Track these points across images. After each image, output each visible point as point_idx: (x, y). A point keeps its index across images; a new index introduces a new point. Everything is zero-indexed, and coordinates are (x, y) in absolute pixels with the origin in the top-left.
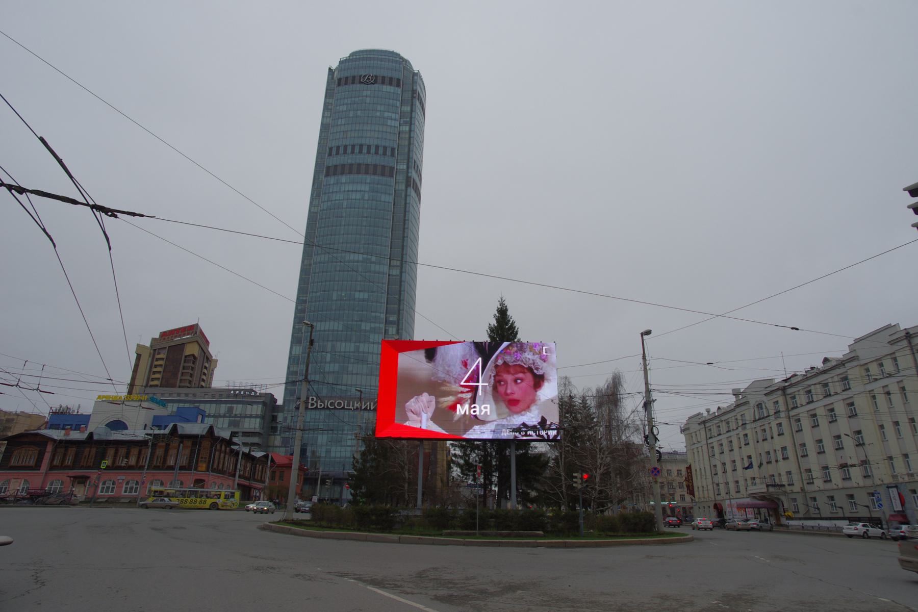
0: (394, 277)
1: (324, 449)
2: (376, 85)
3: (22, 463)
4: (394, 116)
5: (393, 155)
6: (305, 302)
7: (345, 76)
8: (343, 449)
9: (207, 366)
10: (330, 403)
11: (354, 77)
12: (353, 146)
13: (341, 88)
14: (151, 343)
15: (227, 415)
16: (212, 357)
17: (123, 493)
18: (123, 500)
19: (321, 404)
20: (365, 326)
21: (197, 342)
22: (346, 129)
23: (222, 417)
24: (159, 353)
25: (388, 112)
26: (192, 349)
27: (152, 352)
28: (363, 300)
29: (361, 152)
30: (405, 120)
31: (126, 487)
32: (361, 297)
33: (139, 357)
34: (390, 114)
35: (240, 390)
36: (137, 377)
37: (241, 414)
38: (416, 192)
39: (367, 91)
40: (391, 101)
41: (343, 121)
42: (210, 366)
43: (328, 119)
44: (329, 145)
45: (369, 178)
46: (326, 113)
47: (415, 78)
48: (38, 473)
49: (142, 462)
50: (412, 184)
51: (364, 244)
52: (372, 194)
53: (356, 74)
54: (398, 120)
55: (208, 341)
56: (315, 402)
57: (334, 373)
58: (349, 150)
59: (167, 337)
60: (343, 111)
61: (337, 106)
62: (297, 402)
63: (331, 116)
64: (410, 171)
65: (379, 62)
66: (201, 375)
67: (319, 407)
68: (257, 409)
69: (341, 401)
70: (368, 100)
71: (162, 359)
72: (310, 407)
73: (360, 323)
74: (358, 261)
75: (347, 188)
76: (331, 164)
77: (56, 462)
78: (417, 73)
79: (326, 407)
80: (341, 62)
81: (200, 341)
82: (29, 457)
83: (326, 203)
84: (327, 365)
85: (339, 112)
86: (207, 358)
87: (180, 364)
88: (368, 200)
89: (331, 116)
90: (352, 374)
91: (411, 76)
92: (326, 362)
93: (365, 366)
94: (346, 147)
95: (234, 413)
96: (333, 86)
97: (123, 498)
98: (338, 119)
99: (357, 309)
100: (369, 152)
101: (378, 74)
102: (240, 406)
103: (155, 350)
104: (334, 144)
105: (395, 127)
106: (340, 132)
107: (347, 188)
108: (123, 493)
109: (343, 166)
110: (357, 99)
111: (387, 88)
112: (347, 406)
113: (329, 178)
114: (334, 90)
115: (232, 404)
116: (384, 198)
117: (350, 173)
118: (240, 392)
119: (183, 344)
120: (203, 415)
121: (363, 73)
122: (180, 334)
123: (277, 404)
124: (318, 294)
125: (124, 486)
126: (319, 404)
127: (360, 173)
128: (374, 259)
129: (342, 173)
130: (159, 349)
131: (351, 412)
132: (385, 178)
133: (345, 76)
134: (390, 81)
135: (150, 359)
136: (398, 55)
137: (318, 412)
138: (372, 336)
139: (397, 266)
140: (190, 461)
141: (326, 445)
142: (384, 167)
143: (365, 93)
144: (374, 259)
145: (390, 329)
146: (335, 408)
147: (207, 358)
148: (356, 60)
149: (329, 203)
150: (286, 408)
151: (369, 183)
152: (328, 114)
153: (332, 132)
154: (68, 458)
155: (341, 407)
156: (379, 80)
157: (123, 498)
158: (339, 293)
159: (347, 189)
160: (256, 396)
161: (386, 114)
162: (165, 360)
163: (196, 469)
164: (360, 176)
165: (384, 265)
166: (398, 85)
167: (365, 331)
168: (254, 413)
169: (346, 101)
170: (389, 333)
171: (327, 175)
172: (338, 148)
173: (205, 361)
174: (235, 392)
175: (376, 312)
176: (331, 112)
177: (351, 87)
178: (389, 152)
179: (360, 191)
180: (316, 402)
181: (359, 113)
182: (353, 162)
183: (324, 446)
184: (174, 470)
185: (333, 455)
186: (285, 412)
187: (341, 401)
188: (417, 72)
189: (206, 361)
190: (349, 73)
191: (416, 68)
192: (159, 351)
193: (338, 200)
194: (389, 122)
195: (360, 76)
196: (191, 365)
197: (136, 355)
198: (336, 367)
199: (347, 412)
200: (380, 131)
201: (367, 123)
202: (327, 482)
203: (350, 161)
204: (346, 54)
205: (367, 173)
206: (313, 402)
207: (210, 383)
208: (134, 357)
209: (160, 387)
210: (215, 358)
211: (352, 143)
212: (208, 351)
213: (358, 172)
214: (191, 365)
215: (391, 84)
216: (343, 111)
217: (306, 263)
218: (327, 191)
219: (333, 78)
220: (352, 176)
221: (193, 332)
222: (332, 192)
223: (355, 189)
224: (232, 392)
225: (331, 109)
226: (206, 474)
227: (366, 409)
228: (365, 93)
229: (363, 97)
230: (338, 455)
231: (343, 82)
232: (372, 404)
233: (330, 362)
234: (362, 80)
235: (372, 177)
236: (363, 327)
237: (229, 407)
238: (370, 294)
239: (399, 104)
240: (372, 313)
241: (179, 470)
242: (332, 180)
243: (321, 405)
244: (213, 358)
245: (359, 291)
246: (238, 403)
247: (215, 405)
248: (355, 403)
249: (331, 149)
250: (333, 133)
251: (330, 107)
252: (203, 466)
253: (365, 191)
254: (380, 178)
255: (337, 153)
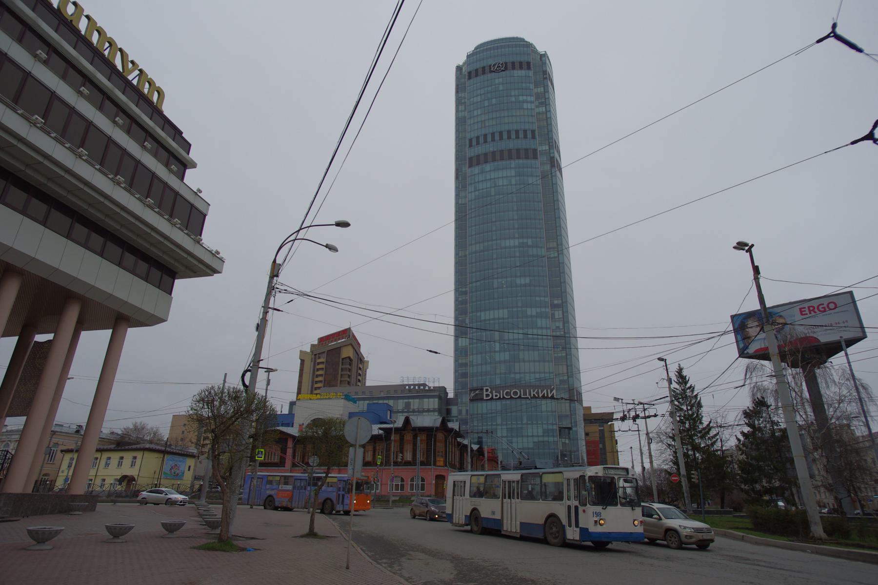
2: (507, 72)
3: (268, 460)
4: (529, 99)
5: (534, 137)
6: (465, 293)
11: (484, 68)
12: (493, 134)
13: (472, 80)
14: (311, 349)
15: (406, 410)
16: (364, 358)
19: (496, 394)
21: (351, 344)
22: (483, 119)
24: (319, 358)
25: (523, 96)
26: (347, 352)
27: (313, 356)
28: (525, 285)
29: (501, 138)
30: (540, 101)
32: (523, 282)
33: (302, 362)
34: (525, 98)
35: (414, 385)
36: (303, 381)
37: (419, 409)
38: (560, 172)
39: (498, 79)
40: (524, 85)
41: (479, 112)
42: (363, 367)
43: (463, 113)
44: (468, 136)
45: (513, 163)
47: (543, 59)
48: (283, 470)
50: (554, 164)
51: (518, 229)
52: (518, 178)
53: (485, 64)
54: (534, 103)
56: (490, 392)
57: (505, 362)
58: (489, 138)
59: (324, 343)
61: (470, 98)
62: (470, 394)
64: (551, 151)
65: (507, 49)
66: (357, 376)
67: (494, 397)
68: (434, 403)
70: (501, 87)
71: (322, 363)
74: (514, 247)
75: (493, 175)
76: (472, 155)
78: (544, 54)
79: (502, 397)
80: (468, 56)
81: (353, 344)
83: (473, 194)
84: (497, 354)
85: (474, 104)
88: (516, 185)
90: (524, 361)
91: (539, 57)
92: (495, 352)
93: (536, 353)
95: (412, 408)
96: (463, 80)
98: (474, 110)
99: (520, 294)
100: (509, 137)
101: (507, 61)
102: (417, 401)
103: (315, 355)
104: (473, 135)
105: (531, 109)
106: (478, 122)
107: (493, 175)
109: (486, 155)
110: (490, 88)
111: (518, 73)
112: (523, 395)
113: (473, 169)
114: (465, 84)
115: (378, 400)
117: (494, 160)
118: (414, 388)
119: (340, 348)
121: (491, 62)
122: (335, 338)
124: (478, 284)
126: (494, 394)
127: (503, 159)
128: (530, 242)
129: (486, 162)
130: (319, 354)
131: (528, 401)
132: (529, 161)
133: (475, 68)
134: (512, 66)
135: (313, 363)
136: (522, 40)
137: (494, 403)
139: (554, 248)
140: (428, 457)
142: (526, 150)
143: (497, 81)
144: (530, 242)
146: (511, 397)
148: (480, 52)
149: (477, 193)
150: (459, 400)
151: (515, 168)
152: (462, 108)
154: (297, 455)
155: (518, 396)
156: (510, 66)
158: (500, 280)
159: (492, 177)
160: (430, 390)
161: (521, 98)
163: (435, 464)
164: (504, 162)
165: (541, 247)
166: (529, 68)
167: (532, 316)
168: (431, 407)
169: (479, 92)
171: (471, 166)
172: (478, 138)
173: (359, 362)
174: (419, 387)
177: (481, 78)
178: (529, 135)
179: (507, 177)
180: (491, 392)
181: (494, 101)
182: (495, 150)
183: (504, 437)
184: (416, 465)
187: (517, 390)
188: (544, 53)
189: (358, 363)
190: (479, 65)
191: (541, 49)
192: (320, 356)
195: (490, 66)
196: (348, 366)
197: (300, 360)
198: (506, 356)
199: (524, 401)
200: (514, 116)
203: (491, 149)
204: (471, 48)
205: (510, 158)
207: (365, 383)
211: (491, 131)
213: (502, 159)
214: (348, 366)
215: (521, 68)
216: (477, 102)
217: (460, 255)
218: (473, 182)
219: (461, 73)
220: (496, 164)
221: (347, 336)
223: (505, 175)
224: (407, 387)
225: (465, 102)
227: (543, 397)
228: (497, 81)
229: (495, 85)
231: (473, 74)
232: (549, 391)
233: (500, 351)
234: (492, 69)
235: (517, 161)
237: (406, 402)
239: (532, 86)
241: (421, 465)
242: (476, 170)
243: (496, 396)
246: (413, 397)
247: (418, 400)
248: (532, 390)
249: (471, 140)
251: (463, 101)
252: (440, 461)
253: (511, 176)
254: (525, 161)
255: (478, 143)
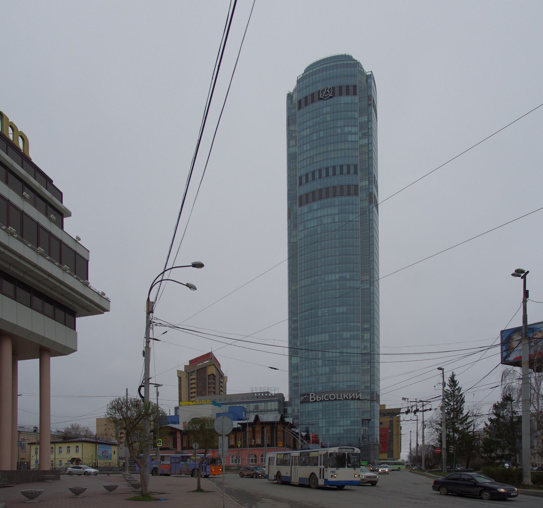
0: (366, 290)
1: (324, 429)
2: (335, 99)
6: (296, 321)
7: (311, 94)
8: (338, 428)
9: (222, 381)
10: (326, 397)
13: (301, 110)
15: (256, 411)
16: (224, 375)
17: (231, 463)
18: (232, 468)
20: (346, 335)
21: (214, 365)
22: (312, 155)
23: (252, 412)
24: (192, 375)
25: (348, 126)
26: (211, 370)
27: (187, 374)
30: (363, 132)
31: (232, 459)
32: (341, 311)
33: (180, 378)
34: (350, 128)
42: (224, 381)
44: (299, 175)
45: (337, 200)
46: (291, 142)
47: (369, 81)
49: (185, 444)
55: (219, 364)
56: (314, 397)
59: (194, 364)
60: (307, 136)
61: (300, 132)
63: (296, 144)
66: (220, 388)
67: (317, 400)
68: (275, 405)
69: (333, 394)
70: (328, 117)
71: (194, 379)
72: (311, 401)
73: (342, 333)
74: (336, 280)
77: (185, 445)
79: (323, 400)
82: (168, 442)
84: (320, 369)
86: (221, 376)
87: (206, 381)
89: (296, 144)
92: (319, 367)
94: (327, 169)
95: (260, 409)
96: (293, 111)
97: (232, 466)
102: (263, 404)
103: (189, 373)
104: (303, 172)
108: (231, 463)
110: (318, 119)
112: (338, 398)
113: (303, 207)
115: (239, 404)
116: (351, 217)
117: (321, 198)
118: (261, 395)
119: (206, 367)
120: (245, 411)
121: (320, 87)
123: (285, 401)
124: (307, 313)
125: (231, 459)
128: (348, 276)
131: (341, 402)
135: (187, 379)
138: (352, 342)
139: (367, 280)
141: (326, 426)
144: (348, 276)
145: (365, 335)
146: (330, 400)
147: (221, 375)
148: (315, 73)
149: (306, 231)
151: (338, 205)
152: (293, 143)
153: (299, 160)
157: (232, 466)
161: (346, 129)
162: (196, 379)
163: (277, 446)
168: (273, 408)
169: (308, 123)
170: (365, 339)
171: (300, 205)
175: (354, 322)
176: (296, 140)
177: (311, 107)
179: (331, 215)
183: (324, 427)
185: (331, 432)
186: (292, 406)
188: (370, 73)
190: (307, 92)
191: (367, 69)
193: (312, 227)
194: (350, 138)
197: (178, 377)
199: (338, 402)
201: (330, 143)
202: (451, 448)
203: (319, 187)
204: (300, 72)
206: (313, 397)
208: (177, 379)
209: (197, 396)
210: (226, 376)
212: (221, 370)
220: (322, 201)
221: (209, 358)
222: (307, 220)
225: (296, 137)
226: (284, 449)
227: (352, 399)
228: (325, 110)
230: (335, 432)
232: (356, 394)
233: (322, 367)
234: (320, 96)
236: (345, 336)
237: (255, 405)
238: (348, 307)
240: (351, 324)
242: (305, 209)
243: (319, 399)
244: (224, 376)
245: (339, 306)
246: (261, 402)
249: (301, 178)
250: (301, 161)
251: (294, 135)
254: (347, 198)
